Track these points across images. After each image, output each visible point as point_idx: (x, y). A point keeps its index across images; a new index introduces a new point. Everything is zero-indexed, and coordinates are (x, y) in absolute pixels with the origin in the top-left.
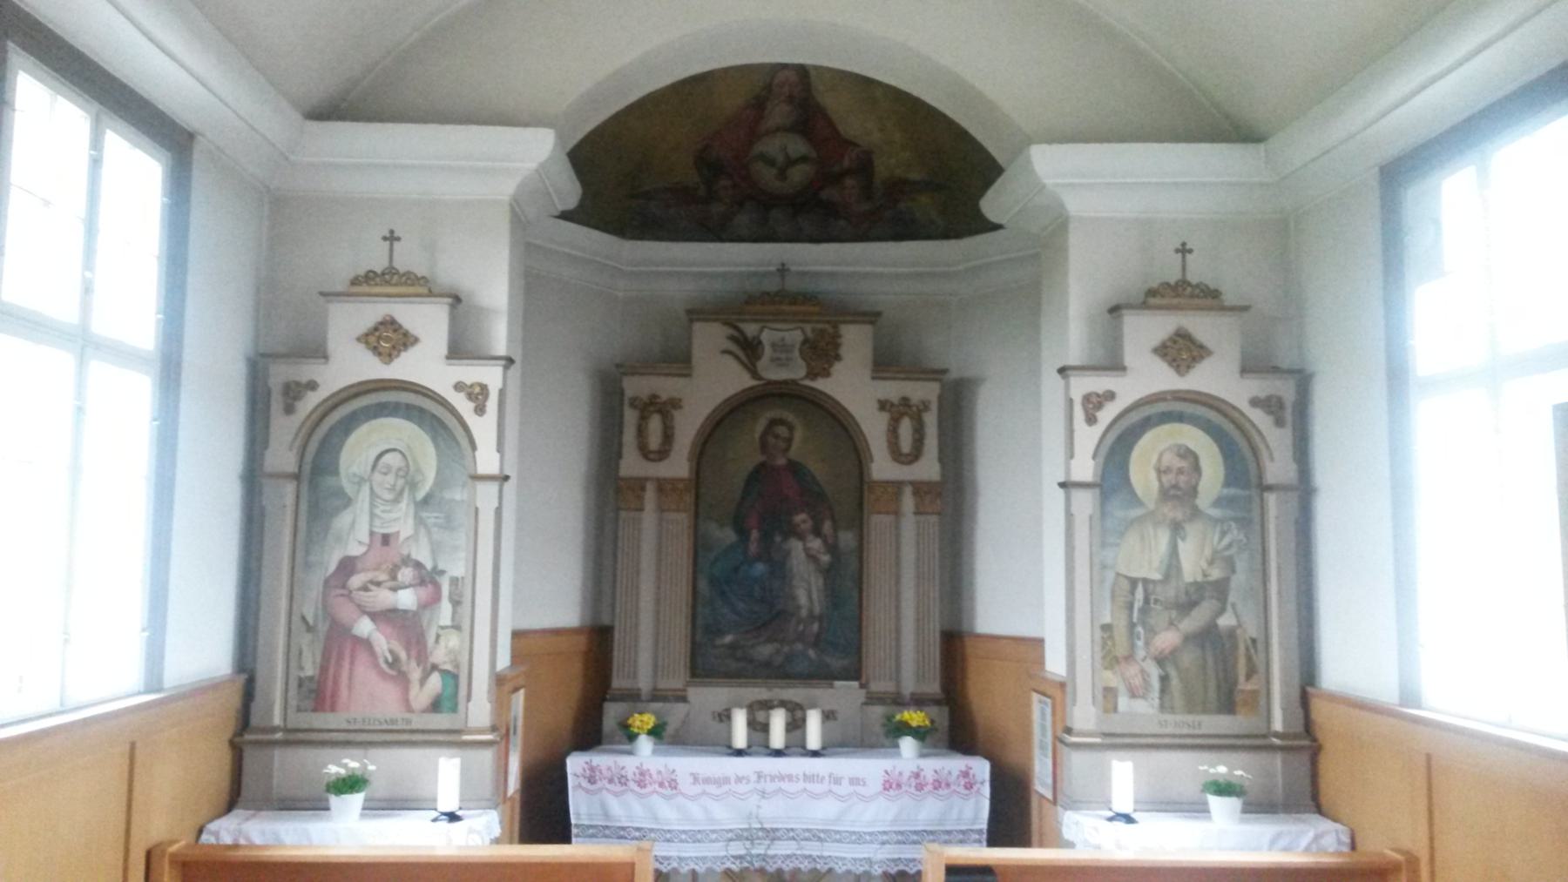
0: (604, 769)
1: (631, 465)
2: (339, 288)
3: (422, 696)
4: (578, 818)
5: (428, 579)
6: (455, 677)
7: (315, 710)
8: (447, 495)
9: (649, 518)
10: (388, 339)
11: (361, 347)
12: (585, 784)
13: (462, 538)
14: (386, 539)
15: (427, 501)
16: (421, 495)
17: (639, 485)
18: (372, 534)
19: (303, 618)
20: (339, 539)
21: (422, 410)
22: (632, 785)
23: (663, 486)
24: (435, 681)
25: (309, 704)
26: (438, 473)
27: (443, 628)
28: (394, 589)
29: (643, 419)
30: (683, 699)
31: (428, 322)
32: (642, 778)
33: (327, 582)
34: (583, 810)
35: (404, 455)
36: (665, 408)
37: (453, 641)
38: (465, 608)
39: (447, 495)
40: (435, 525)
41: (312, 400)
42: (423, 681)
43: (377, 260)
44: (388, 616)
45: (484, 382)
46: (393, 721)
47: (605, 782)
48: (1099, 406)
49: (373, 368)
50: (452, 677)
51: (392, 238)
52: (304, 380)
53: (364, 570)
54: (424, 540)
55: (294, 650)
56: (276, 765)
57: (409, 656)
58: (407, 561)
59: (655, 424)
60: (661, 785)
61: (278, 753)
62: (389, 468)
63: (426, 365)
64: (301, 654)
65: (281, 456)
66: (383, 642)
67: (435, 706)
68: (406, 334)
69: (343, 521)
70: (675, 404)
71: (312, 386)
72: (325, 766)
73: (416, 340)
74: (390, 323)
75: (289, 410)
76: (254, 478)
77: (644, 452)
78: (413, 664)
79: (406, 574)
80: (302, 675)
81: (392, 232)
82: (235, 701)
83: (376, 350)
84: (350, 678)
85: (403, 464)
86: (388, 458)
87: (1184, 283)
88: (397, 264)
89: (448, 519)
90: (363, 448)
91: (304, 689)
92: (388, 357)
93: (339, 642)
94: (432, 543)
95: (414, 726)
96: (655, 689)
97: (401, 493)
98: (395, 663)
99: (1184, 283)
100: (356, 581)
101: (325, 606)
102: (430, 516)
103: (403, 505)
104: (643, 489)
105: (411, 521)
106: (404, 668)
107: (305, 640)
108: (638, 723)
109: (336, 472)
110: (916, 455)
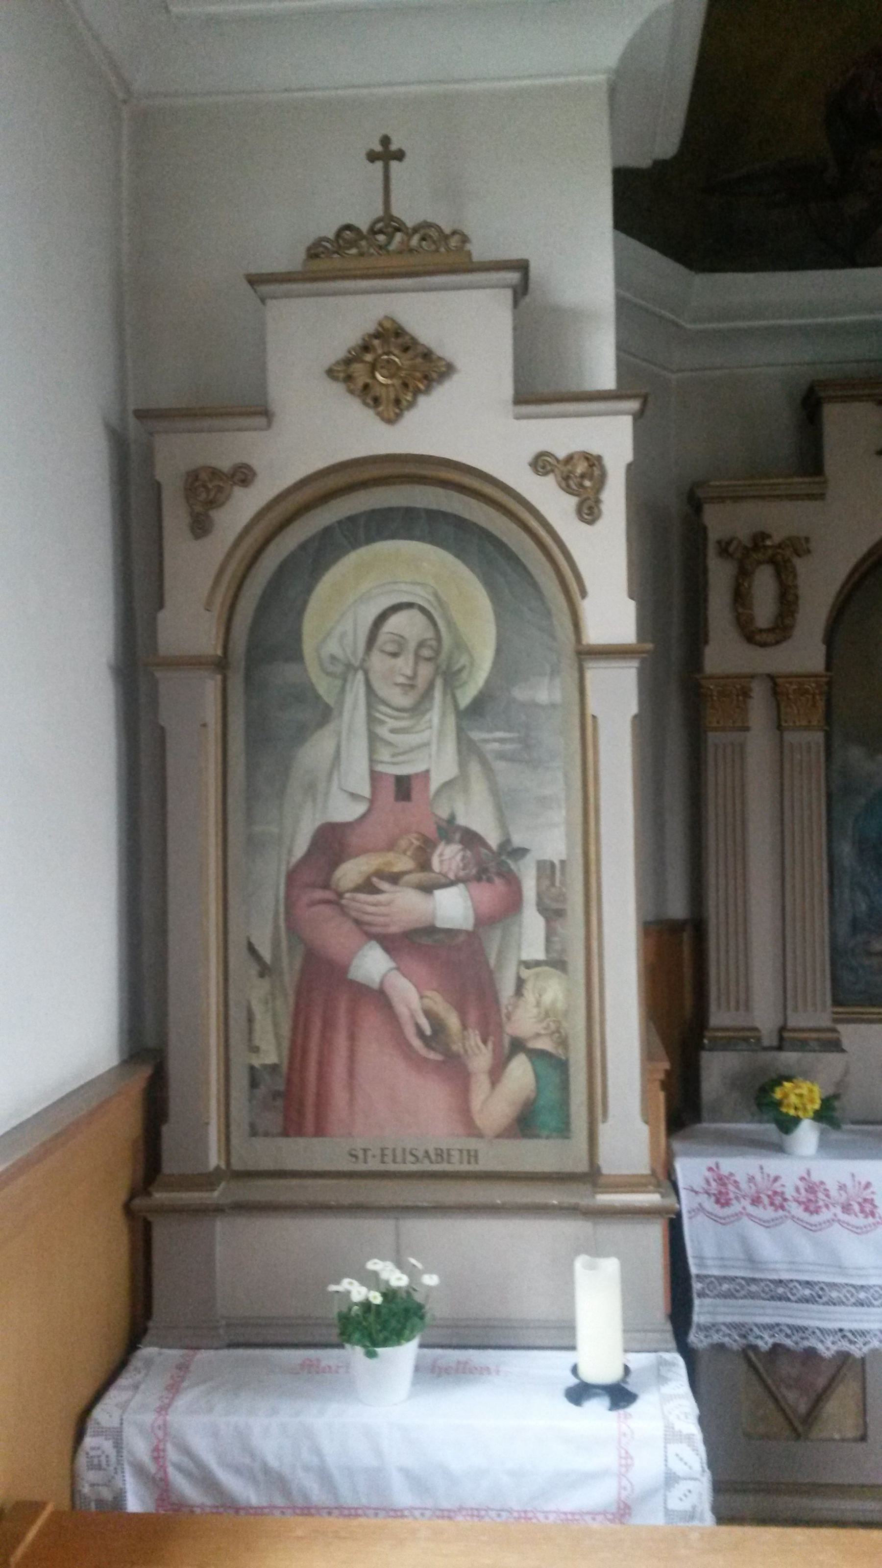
0: (741, 1178)
1: (725, 653)
2: (280, 266)
3: (495, 1105)
4: (700, 1266)
5: (492, 865)
6: (562, 1066)
7: (285, 1134)
8: (520, 693)
9: (758, 742)
10: (393, 370)
11: (338, 388)
12: (709, 1205)
13: (556, 783)
14: (404, 787)
15: (477, 709)
16: (466, 697)
17: (738, 689)
18: (375, 777)
19: (251, 949)
20: (311, 788)
21: (461, 524)
22: (797, 1210)
23: (775, 684)
24: (520, 1074)
25: (273, 1119)
26: (498, 651)
27: (528, 965)
28: (428, 889)
29: (744, 573)
30: (835, 1046)
31: (467, 326)
32: (812, 1196)
33: (291, 877)
34: (709, 1251)
35: (422, 609)
36: (781, 558)
37: (553, 991)
38: (573, 929)
39: (520, 693)
40: (501, 756)
41: (243, 507)
42: (496, 1073)
43: (351, 201)
44: (415, 943)
45: (594, 449)
46: (442, 1155)
47: (746, 1203)
48: (567, 483)
49: (368, 436)
50: (553, 1065)
51: (386, 154)
52: (225, 464)
53: (364, 851)
54: (478, 787)
55: (237, 1015)
56: (219, 1250)
57: (465, 1027)
58: (449, 830)
59: (764, 586)
60: (846, 1208)
61: (220, 1226)
62: (400, 641)
63: (471, 422)
64: (250, 1020)
65: (189, 624)
66: (409, 996)
67: (525, 1123)
68: (427, 355)
69: (316, 751)
70: (799, 546)
71: (243, 475)
72: (327, 1285)
73: (447, 370)
74: (391, 334)
75: (201, 526)
76: (138, 669)
77: (750, 635)
78: (474, 1038)
79: (448, 857)
80: (257, 1062)
81: (386, 141)
82: (126, 1122)
83: (369, 396)
84: (351, 1073)
85: (430, 634)
86: (395, 622)
87: (389, 224)
88: (395, 212)
89: (526, 743)
90: (364, 596)
91: (262, 1090)
92: (392, 406)
93: (320, 989)
94: (494, 791)
95: (485, 1164)
96: (783, 1029)
97: (428, 694)
98: (437, 1035)
99: (389, 224)
100: (350, 872)
101: (292, 927)
102: (490, 738)
103: (435, 715)
104: (745, 693)
105: (450, 746)
106: (456, 1047)
107: (255, 992)
108: (793, 1099)
109: (297, 656)
110: (782, 628)
